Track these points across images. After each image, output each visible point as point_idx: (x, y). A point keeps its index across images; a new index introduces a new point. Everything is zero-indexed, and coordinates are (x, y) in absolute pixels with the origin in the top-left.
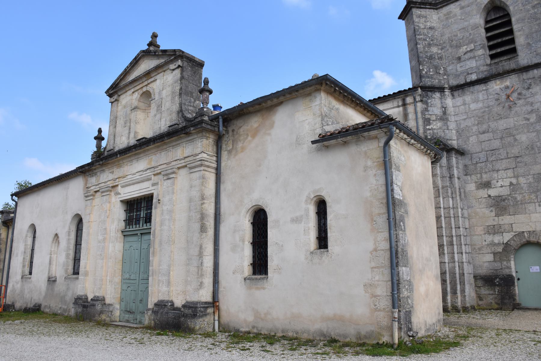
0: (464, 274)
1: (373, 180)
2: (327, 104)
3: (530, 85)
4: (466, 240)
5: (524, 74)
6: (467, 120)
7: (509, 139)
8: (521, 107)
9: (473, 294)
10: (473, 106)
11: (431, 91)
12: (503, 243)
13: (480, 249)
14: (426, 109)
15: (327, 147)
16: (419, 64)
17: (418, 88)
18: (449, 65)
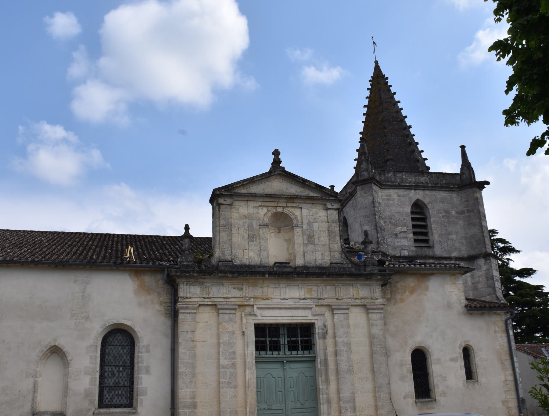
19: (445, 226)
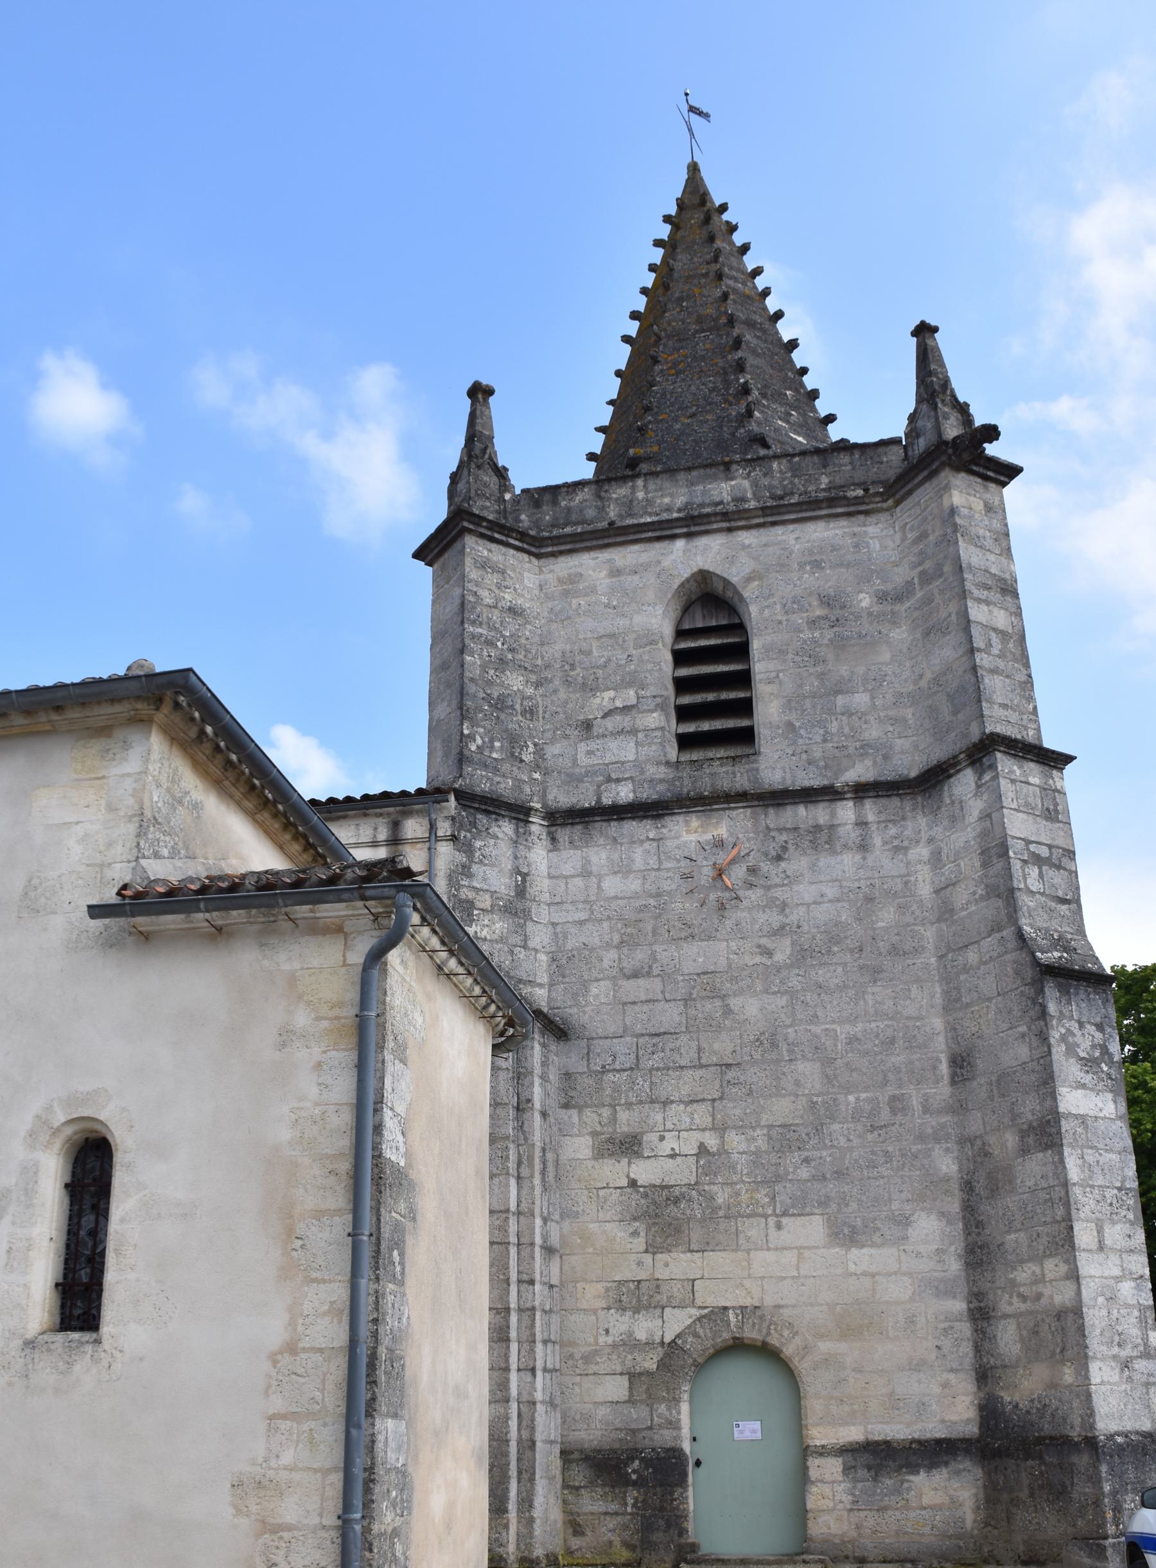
0: (533, 1443)
1: (308, 1085)
2: (163, 779)
3: (784, 849)
4: (549, 1324)
5: (771, 811)
6: (589, 926)
7: (708, 1006)
8: (753, 913)
9: (557, 1514)
10: (612, 885)
11: (487, 812)
12: (662, 1343)
13: (587, 1359)
14: (464, 867)
15: (146, 937)
16: (463, 718)
17: (447, 792)
18: (553, 741)
19: (818, 660)
